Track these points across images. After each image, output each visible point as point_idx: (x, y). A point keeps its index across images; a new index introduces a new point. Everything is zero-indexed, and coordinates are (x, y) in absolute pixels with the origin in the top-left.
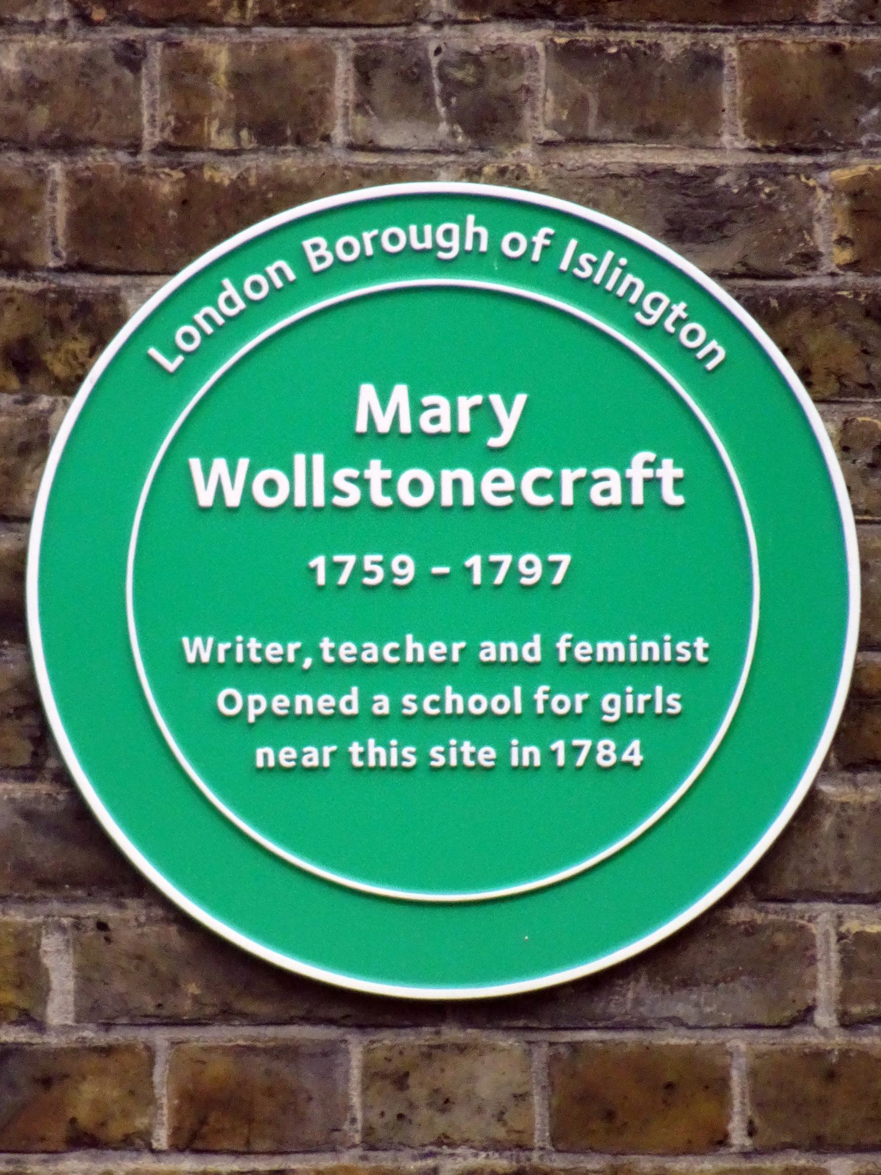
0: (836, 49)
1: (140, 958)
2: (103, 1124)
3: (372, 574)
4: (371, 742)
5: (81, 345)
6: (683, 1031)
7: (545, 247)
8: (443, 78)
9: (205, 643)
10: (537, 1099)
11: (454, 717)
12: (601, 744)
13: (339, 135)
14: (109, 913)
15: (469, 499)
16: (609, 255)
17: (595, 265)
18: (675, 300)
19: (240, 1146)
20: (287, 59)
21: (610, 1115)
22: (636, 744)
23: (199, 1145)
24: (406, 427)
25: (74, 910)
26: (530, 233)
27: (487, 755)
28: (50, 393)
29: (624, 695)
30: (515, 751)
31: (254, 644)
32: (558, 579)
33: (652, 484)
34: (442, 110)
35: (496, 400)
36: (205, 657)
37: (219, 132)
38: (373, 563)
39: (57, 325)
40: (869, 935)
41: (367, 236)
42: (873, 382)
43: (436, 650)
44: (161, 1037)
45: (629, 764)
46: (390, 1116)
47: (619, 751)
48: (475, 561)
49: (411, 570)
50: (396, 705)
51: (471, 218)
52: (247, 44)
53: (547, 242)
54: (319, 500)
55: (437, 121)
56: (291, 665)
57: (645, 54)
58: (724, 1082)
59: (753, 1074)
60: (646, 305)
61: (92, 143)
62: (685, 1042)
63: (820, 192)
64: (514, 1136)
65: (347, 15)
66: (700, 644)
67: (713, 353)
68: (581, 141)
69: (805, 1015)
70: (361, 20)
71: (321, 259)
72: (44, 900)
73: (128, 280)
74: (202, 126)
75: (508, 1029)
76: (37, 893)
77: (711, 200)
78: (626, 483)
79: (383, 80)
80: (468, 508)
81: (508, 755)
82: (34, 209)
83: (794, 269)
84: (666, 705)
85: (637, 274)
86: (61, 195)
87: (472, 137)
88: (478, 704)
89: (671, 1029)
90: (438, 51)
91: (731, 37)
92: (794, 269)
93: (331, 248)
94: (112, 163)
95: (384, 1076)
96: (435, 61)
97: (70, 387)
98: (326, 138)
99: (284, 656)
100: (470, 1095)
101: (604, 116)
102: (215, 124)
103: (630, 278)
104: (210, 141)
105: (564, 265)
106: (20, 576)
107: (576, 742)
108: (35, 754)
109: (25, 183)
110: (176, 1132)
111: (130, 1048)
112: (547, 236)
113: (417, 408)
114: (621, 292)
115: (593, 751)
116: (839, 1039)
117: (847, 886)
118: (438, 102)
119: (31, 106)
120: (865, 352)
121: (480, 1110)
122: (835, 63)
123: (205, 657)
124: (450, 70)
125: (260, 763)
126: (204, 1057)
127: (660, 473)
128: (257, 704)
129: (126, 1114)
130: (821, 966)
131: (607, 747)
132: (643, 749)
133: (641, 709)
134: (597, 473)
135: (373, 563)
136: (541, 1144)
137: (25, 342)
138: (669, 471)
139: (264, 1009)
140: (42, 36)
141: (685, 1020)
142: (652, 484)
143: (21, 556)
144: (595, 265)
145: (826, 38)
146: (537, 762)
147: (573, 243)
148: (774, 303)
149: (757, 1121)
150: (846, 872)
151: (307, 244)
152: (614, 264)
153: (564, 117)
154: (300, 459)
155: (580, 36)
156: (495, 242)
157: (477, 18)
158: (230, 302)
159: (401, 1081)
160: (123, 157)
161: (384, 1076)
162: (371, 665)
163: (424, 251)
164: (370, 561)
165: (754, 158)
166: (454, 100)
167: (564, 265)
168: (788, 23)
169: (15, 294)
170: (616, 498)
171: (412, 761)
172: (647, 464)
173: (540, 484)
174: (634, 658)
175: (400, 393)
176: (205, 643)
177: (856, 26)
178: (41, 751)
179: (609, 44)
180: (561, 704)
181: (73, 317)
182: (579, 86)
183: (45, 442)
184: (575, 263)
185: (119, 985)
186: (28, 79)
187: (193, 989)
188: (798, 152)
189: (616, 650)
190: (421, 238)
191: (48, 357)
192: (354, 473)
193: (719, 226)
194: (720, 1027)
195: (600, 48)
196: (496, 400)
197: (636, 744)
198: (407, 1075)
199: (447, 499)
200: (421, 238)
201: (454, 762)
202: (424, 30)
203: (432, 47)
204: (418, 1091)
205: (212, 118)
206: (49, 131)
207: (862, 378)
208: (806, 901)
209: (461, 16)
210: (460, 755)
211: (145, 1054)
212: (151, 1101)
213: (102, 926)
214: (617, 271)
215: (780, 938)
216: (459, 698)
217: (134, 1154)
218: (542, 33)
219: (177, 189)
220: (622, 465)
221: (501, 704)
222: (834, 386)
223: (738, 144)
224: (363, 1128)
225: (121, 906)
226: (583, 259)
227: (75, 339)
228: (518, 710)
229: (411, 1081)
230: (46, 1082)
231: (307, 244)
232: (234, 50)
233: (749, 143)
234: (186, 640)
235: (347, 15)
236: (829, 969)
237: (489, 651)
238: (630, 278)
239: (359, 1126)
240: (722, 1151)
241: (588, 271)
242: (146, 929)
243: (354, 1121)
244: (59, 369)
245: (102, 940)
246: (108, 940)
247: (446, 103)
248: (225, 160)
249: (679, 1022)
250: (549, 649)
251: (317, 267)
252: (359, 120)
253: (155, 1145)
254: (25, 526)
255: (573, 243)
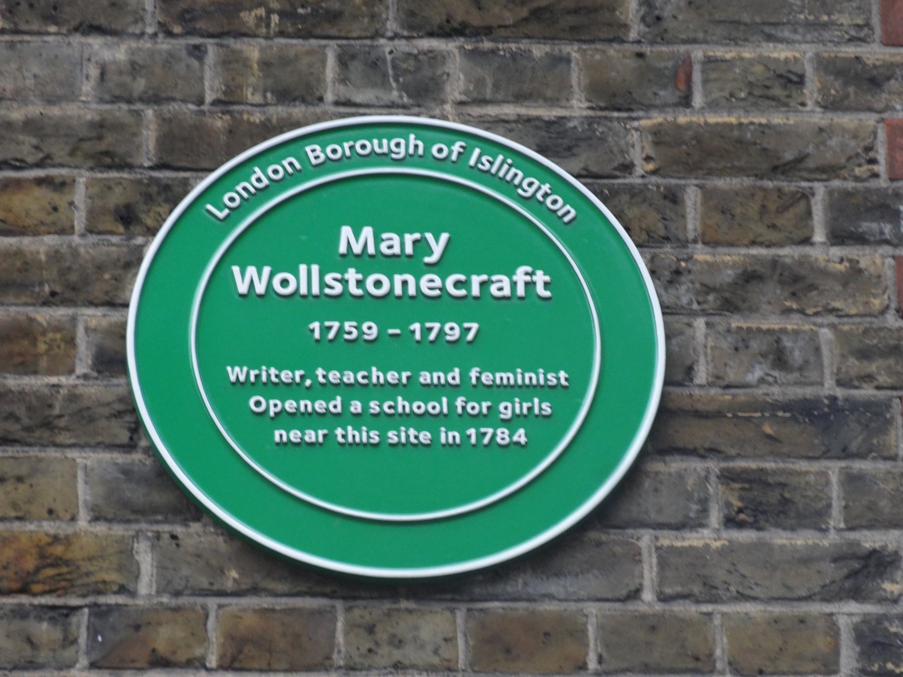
0: (640, 55)
1: (198, 556)
2: (174, 653)
3: (350, 333)
4: (350, 428)
5: (167, 207)
6: (555, 603)
7: (460, 154)
8: (394, 67)
9: (241, 371)
10: (461, 642)
11: (404, 415)
12: (499, 431)
13: (329, 97)
14: (179, 530)
15: (412, 291)
16: (500, 158)
17: (491, 163)
18: (543, 182)
19: (264, 666)
20: (296, 55)
21: (508, 651)
22: (522, 431)
23: (237, 665)
24: (371, 250)
25: (156, 527)
26: (450, 144)
27: (425, 437)
28: (144, 236)
29: (513, 404)
30: (443, 435)
31: (273, 371)
32: (470, 336)
33: (530, 285)
34: (394, 85)
35: (429, 236)
36: (242, 378)
37: (253, 94)
38: (350, 326)
39: (149, 198)
40: (677, 548)
41: (346, 145)
42: (670, 236)
43: (392, 377)
44: (212, 603)
45: (518, 443)
46: (363, 650)
47: (510, 436)
48: (416, 326)
49: (374, 332)
50: (365, 407)
51: (412, 137)
52: (271, 47)
53: (461, 150)
54: (315, 290)
55: (391, 89)
56: (298, 384)
57: (521, 55)
58: (584, 631)
59: (601, 627)
60: (525, 185)
61: (173, 99)
62: (557, 608)
63: (633, 132)
64: (446, 663)
65: (333, 32)
66: (562, 374)
67: (568, 212)
68: (482, 102)
69: (635, 594)
70: (343, 34)
71: (317, 157)
72: (137, 521)
73: (194, 174)
74: (242, 91)
75: (441, 600)
76: (132, 517)
77: (563, 134)
78: (514, 284)
79: (356, 67)
80: (412, 298)
81: (439, 437)
82: (135, 135)
83: (617, 173)
84: (541, 409)
85: (517, 168)
86: (153, 127)
87: (412, 99)
88: (419, 407)
89: (547, 601)
90: (391, 52)
91: (576, 47)
92: (617, 173)
93: (323, 151)
94: (185, 110)
95: (359, 626)
96: (389, 57)
97: (153, 232)
98: (321, 99)
99: (293, 379)
100: (415, 639)
101: (496, 87)
102: (250, 90)
103: (513, 170)
104: (247, 98)
105: (472, 162)
106: (123, 337)
107: (483, 430)
108: (131, 439)
109: (129, 120)
110: (222, 657)
111: (192, 609)
112: (462, 147)
113: (378, 240)
114: (508, 178)
115: (494, 436)
116: (659, 607)
117: (661, 519)
118: (391, 80)
119: (135, 78)
120: (665, 219)
121: (422, 647)
122: (640, 62)
123: (242, 378)
124: (398, 62)
125: (277, 439)
126: (240, 614)
127: (535, 278)
128: (276, 405)
129: (188, 646)
130: (646, 566)
131: (503, 433)
132: (526, 435)
133: (525, 411)
134: (494, 278)
135: (350, 326)
136: (463, 667)
137: (128, 207)
138: (540, 278)
139: (280, 587)
140: (142, 41)
141: (556, 595)
142: (530, 285)
143: (124, 326)
144: (491, 163)
145: (636, 48)
146: (458, 441)
147: (477, 151)
148: (606, 192)
149: (605, 655)
150: (660, 511)
151: (308, 149)
152: (503, 162)
153: (471, 88)
154: (303, 268)
155: (481, 45)
156: (427, 149)
157: (415, 35)
158: (259, 180)
159: (370, 629)
160: (192, 107)
161: (359, 626)
162: (350, 385)
163: (384, 154)
164: (347, 326)
165: (591, 113)
166: (401, 79)
167: (472, 162)
168: (610, 41)
169: (123, 180)
170: (507, 292)
171: (376, 440)
172: (527, 274)
173: (458, 284)
174: (520, 382)
175: (367, 232)
176: (241, 371)
177: (653, 43)
178: (135, 437)
179: (499, 49)
180: (473, 408)
181: (158, 193)
182: (479, 72)
183: (140, 260)
184: (479, 160)
185: (185, 571)
186: (133, 64)
187: (234, 574)
188: (619, 110)
189: (508, 379)
190: (380, 146)
191: (143, 216)
192: (338, 276)
193: (569, 149)
194: (579, 600)
195: (494, 52)
196: (429, 236)
197: (522, 431)
198: (374, 626)
199: (398, 291)
200: (380, 146)
201: (403, 440)
202: (382, 41)
203: (387, 50)
204: (382, 635)
205: (248, 86)
206: (145, 92)
207: (662, 232)
208: (634, 528)
209: (406, 33)
210: (408, 437)
211: (201, 611)
212: (205, 640)
213: (174, 537)
214: (506, 167)
215: (618, 549)
216: (407, 404)
217: (194, 671)
218: (458, 43)
219: (226, 125)
220: (510, 273)
221: (434, 408)
222: (644, 236)
223: (582, 106)
224: (345, 657)
225: (187, 526)
226: (484, 159)
227: (160, 205)
228: (445, 410)
229: (376, 630)
230: (137, 627)
231: (308, 149)
232: (262, 50)
233: (589, 104)
234: (229, 369)
235: (333, 32)
236: (651, 567)
237: (425, 377)
238: (513, 170)
239: (342, 655)
240: (582, 672)
241: (488, 165)
242: (203, 539)
243: (339, 652)
244: (149, 222)
245: (174, 545)
246: (178, 545)
247: (397, 81)
248: (257, 109)
249: (551, 597)
250: (464, 376)
251: (314, 161)
252: (342, 89)
253: (208, 665)
254: (125, 310)
255: (477, 151)
